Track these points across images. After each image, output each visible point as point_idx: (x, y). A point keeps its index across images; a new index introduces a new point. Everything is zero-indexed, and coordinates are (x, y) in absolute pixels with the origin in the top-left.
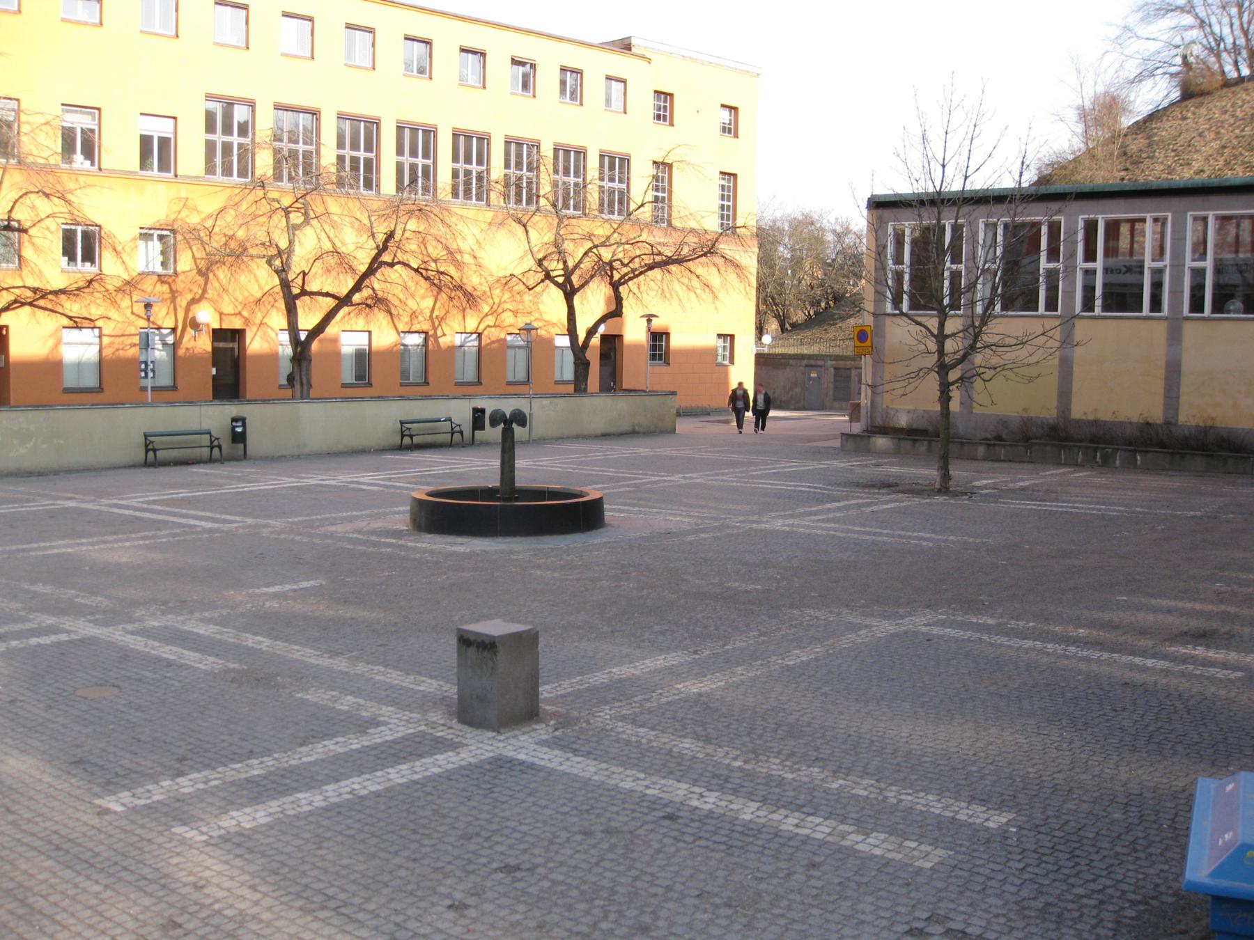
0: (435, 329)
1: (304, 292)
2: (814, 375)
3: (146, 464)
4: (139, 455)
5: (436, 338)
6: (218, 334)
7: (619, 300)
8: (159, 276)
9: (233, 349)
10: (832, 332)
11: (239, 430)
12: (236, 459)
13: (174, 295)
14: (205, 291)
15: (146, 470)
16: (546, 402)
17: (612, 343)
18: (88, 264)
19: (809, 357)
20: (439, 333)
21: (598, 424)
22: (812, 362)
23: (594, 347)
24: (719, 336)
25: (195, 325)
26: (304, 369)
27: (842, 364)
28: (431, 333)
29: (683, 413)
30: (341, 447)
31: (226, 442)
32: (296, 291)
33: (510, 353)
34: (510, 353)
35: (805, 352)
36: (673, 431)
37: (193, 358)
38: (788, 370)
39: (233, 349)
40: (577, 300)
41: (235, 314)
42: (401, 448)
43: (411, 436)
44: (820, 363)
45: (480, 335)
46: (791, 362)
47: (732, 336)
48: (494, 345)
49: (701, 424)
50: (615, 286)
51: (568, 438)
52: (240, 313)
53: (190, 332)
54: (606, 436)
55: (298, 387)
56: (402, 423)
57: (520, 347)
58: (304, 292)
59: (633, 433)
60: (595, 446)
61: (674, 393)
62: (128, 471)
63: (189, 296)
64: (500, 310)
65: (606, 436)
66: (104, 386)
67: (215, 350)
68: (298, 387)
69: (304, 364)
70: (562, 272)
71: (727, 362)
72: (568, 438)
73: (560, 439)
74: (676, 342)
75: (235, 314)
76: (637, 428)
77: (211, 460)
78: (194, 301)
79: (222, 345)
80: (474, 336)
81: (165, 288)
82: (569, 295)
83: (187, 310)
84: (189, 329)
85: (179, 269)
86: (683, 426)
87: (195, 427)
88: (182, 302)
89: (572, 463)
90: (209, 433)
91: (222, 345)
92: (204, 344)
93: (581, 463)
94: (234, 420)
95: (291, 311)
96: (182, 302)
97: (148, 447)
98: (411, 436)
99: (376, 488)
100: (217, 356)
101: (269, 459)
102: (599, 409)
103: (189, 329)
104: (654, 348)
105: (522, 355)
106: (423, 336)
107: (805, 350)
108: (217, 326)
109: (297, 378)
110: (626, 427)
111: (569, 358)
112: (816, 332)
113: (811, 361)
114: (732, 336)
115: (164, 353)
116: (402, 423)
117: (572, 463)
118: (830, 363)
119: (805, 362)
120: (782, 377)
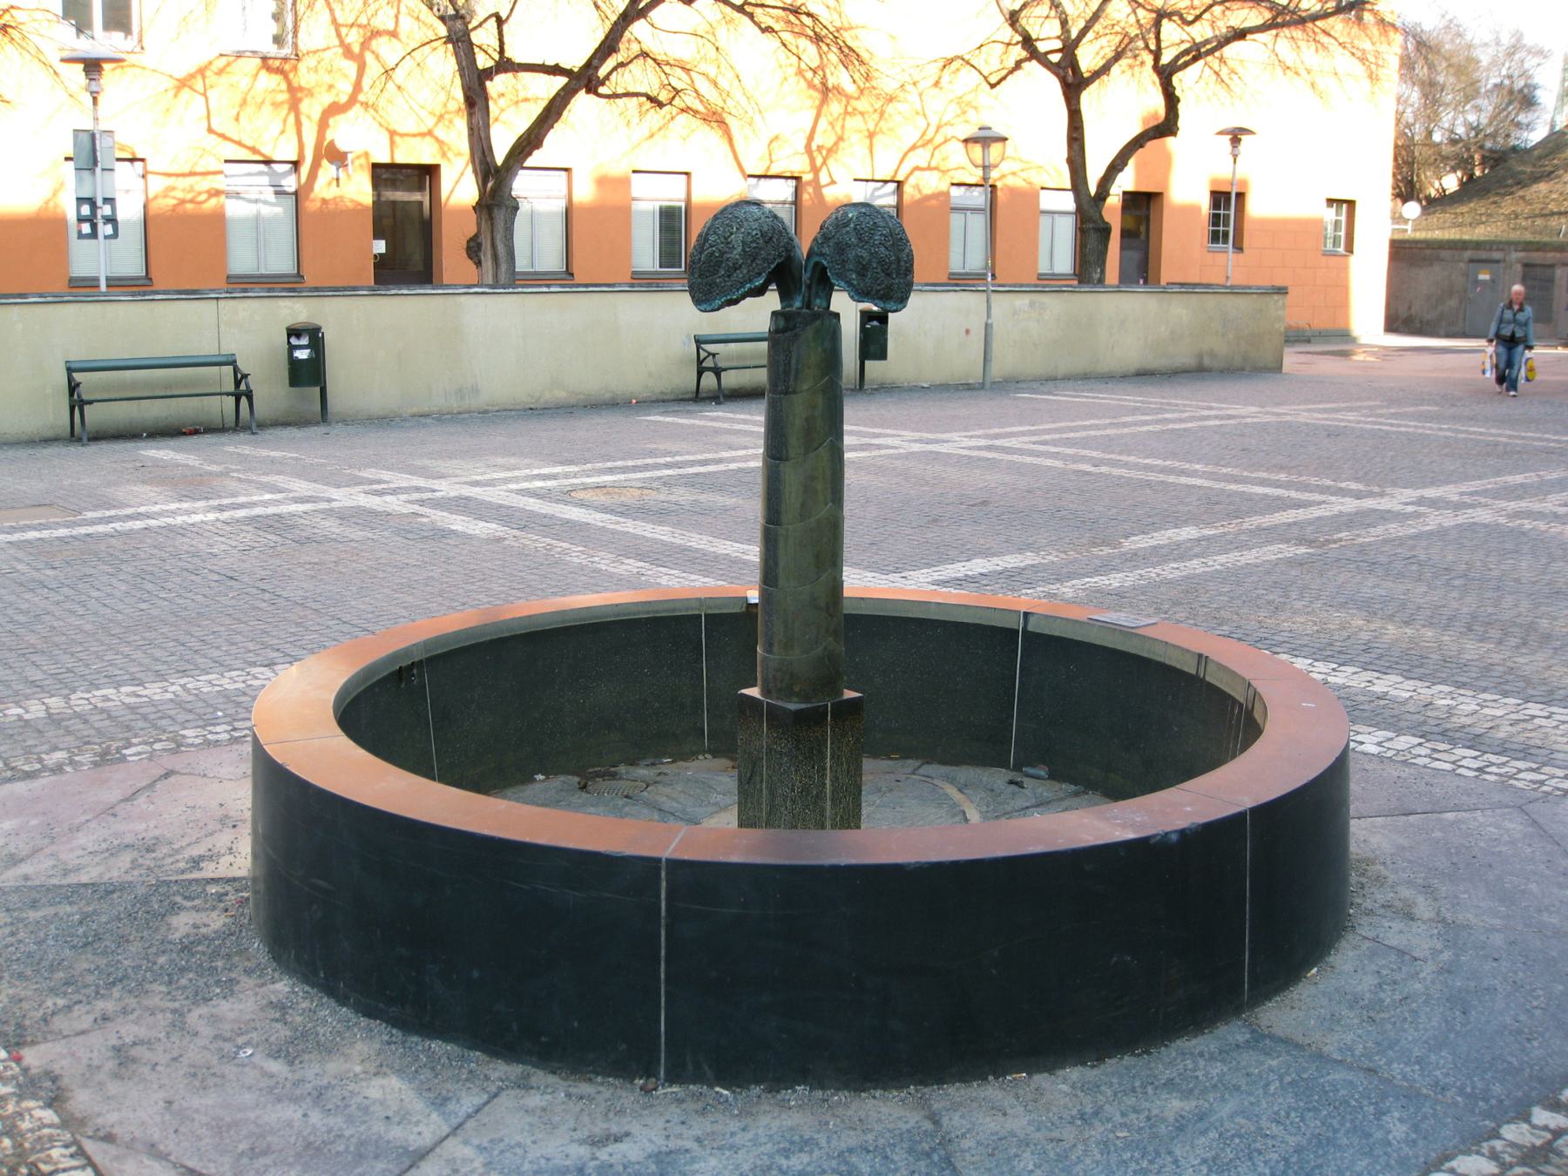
0: (815, 170)
1: (505, 65)
2: (1484, 277)
3: (73, 437)
4: (57, 415)
5: (816, 182)
6: (384, 174)
7: (1171, 100)
8: (264, 59)
9: (421, 203)
10: (1508, 205)
11: (302, 355)
12: (300, 422)
13: (295, 96)
14: (358, 87)
15: (74, 450)
16: (1022, 301)
17: (1143, 204)
18: (118, 36)
19: (1478, 245)
20: (824, 178)
21: (1129, 351)
22: (1483, 255)
23: (1113, 208)
24: (1330, 202)
25: (338, 158)
26: (500, 225)
27: (1536, 257)
28: (807, 177)
29: (1298, 337)
30: (560, 395)
31: (271, 391)
32: (483, 62)
33: (956, 220)
34: (956, 220)
35: (1466, 237)
36: (1277, 368)
37: (333, 214)
38: (1437, 268)
39: (421, 203)
40: (1087, 98)
41: (423, 135)
42: (698, 397)
43: (717, 372)
44: (1496, 255)
45: (900, 184)
46: (1444, 254)
47: (1351, 204)
48: (934, 202)
49: (1303, 358)
50: (1165, 75)
51: (1067, 378)
52: (430, 133)
53: (327, 170)
54: (1144, 375)
55: (488, 263)
56: (699, 342)
57: (974, 210)
58: (505, 65)
59: (1199, 371)
60: (1130, 397)
61: (1282, 291)
62: (23, 453)
63: (325, 100)
64: (939, 139)
65: (1144, 375)
66: (153, 275)
67: (377, 203)
68: (488, 263)
69: (500, 216)
70: (1059, 45)
71: (1341, 250)
72: (1067, 378)
73: (1050, 380)
74: (1256, 208)
75: (423, 135)
76: (1207, 362)
77: (237, 426)
78: (335, 109)
79: (400, 196)
80: (892, 186)
81: (276, 81)
82: (1073, 84)
83: (323, 125)
84: (325, 162)
85: (303, 47)
86: (1292, 359)
87: (207, 348)
88: (312, 109)
89: (1085, 443)
90: (233, 363)
91: (400, 196)
92: (359, 190)
93: (1107, 444)
94: (293, 332)
95: (476, 99)
96: (312, 109)
97: (77, 401)
98: (717, 372)
99: (482, 528)
100: (386, 219)
101: (383, 421)
102: (1126, 320)
103: (325, 162)
104: (1215, 219)
105: (978, 224)
106: (792, 183)
107: (1480, 233)
108: (385, 159)
109: (486, 245)
110: (1183, 356)
111: (1066, 231)
112: (1478, 206)
113: (1480, 255)
114: (1351, 204)
115: (279, 210)
116: (699, 342)
117: (1085, 443)
118: (1515, 256)
119: (1468, 254)
120: (1427, 279)
